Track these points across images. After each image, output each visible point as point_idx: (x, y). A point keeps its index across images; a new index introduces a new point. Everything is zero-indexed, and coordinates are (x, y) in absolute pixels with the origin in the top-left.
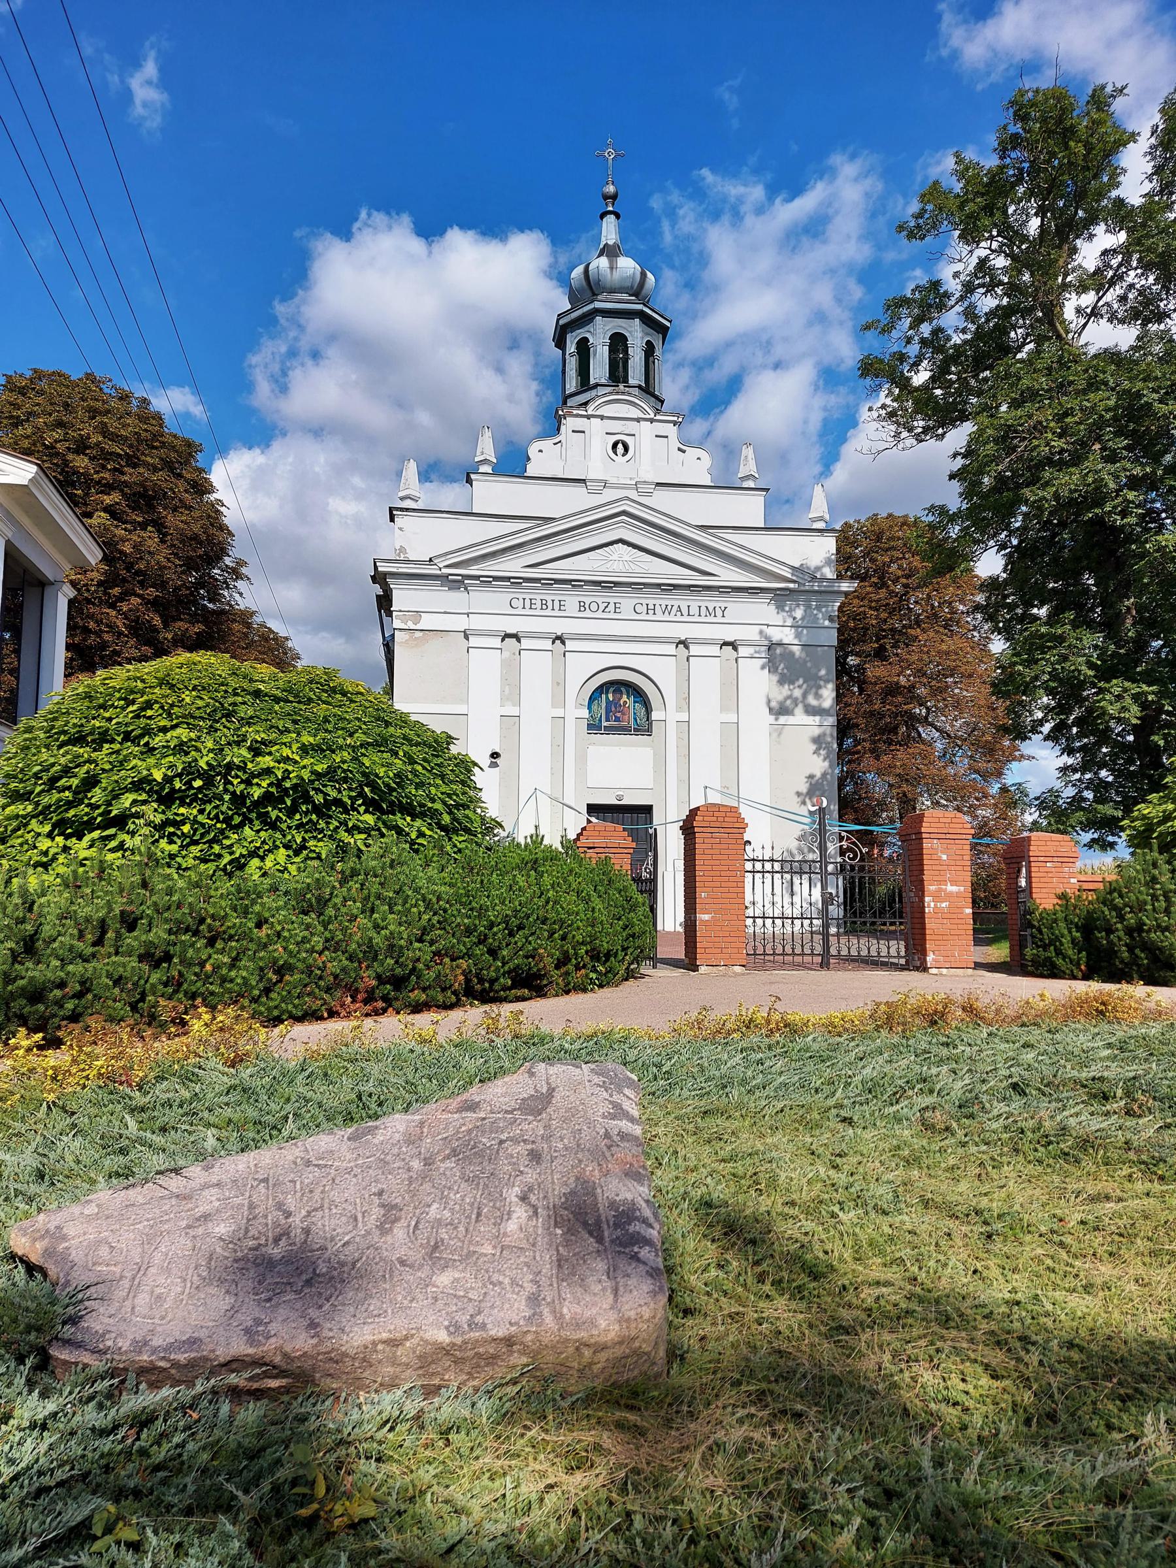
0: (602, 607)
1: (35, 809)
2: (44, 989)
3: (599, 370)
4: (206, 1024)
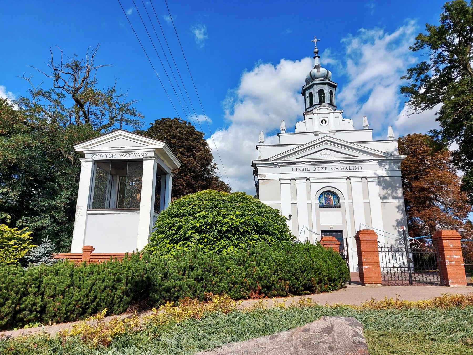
0: (321, 169)
1: (165, 236)
2: (169, 289)
3: (316, 100)
4: (218, 300)
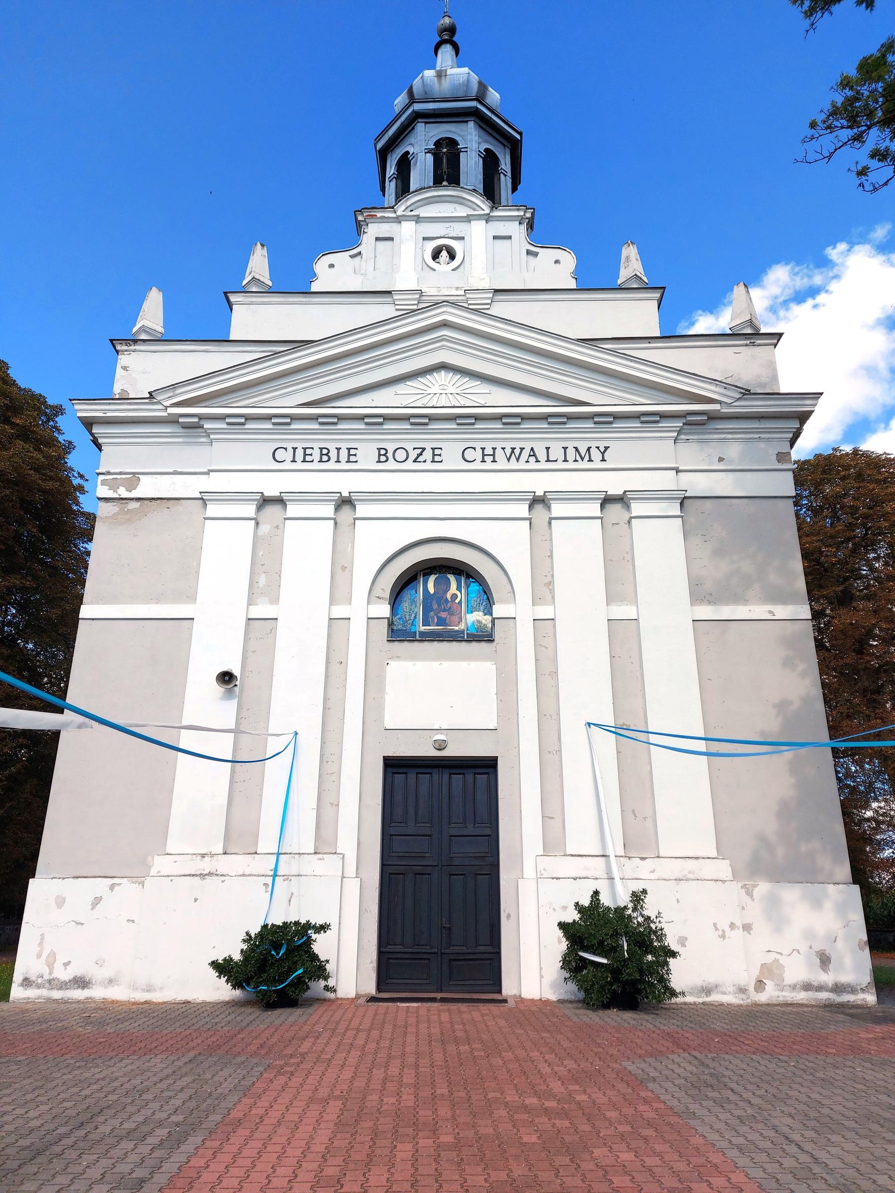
0: (413, 455)
